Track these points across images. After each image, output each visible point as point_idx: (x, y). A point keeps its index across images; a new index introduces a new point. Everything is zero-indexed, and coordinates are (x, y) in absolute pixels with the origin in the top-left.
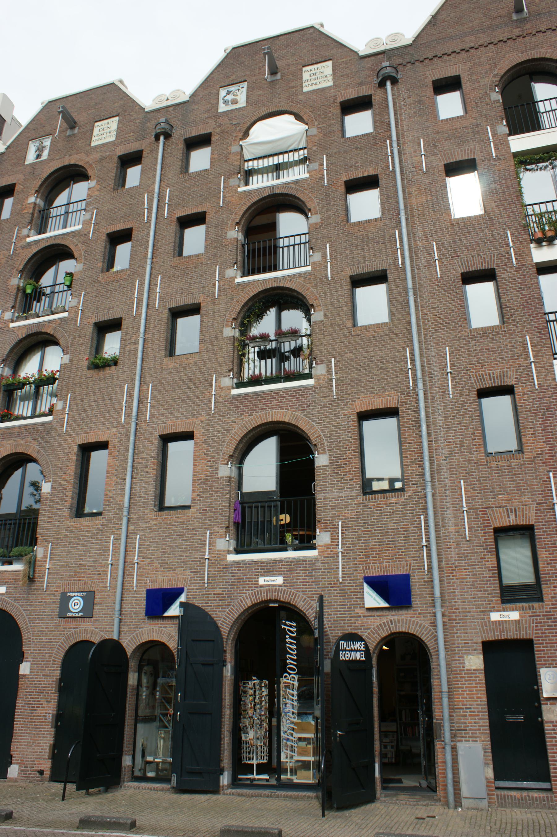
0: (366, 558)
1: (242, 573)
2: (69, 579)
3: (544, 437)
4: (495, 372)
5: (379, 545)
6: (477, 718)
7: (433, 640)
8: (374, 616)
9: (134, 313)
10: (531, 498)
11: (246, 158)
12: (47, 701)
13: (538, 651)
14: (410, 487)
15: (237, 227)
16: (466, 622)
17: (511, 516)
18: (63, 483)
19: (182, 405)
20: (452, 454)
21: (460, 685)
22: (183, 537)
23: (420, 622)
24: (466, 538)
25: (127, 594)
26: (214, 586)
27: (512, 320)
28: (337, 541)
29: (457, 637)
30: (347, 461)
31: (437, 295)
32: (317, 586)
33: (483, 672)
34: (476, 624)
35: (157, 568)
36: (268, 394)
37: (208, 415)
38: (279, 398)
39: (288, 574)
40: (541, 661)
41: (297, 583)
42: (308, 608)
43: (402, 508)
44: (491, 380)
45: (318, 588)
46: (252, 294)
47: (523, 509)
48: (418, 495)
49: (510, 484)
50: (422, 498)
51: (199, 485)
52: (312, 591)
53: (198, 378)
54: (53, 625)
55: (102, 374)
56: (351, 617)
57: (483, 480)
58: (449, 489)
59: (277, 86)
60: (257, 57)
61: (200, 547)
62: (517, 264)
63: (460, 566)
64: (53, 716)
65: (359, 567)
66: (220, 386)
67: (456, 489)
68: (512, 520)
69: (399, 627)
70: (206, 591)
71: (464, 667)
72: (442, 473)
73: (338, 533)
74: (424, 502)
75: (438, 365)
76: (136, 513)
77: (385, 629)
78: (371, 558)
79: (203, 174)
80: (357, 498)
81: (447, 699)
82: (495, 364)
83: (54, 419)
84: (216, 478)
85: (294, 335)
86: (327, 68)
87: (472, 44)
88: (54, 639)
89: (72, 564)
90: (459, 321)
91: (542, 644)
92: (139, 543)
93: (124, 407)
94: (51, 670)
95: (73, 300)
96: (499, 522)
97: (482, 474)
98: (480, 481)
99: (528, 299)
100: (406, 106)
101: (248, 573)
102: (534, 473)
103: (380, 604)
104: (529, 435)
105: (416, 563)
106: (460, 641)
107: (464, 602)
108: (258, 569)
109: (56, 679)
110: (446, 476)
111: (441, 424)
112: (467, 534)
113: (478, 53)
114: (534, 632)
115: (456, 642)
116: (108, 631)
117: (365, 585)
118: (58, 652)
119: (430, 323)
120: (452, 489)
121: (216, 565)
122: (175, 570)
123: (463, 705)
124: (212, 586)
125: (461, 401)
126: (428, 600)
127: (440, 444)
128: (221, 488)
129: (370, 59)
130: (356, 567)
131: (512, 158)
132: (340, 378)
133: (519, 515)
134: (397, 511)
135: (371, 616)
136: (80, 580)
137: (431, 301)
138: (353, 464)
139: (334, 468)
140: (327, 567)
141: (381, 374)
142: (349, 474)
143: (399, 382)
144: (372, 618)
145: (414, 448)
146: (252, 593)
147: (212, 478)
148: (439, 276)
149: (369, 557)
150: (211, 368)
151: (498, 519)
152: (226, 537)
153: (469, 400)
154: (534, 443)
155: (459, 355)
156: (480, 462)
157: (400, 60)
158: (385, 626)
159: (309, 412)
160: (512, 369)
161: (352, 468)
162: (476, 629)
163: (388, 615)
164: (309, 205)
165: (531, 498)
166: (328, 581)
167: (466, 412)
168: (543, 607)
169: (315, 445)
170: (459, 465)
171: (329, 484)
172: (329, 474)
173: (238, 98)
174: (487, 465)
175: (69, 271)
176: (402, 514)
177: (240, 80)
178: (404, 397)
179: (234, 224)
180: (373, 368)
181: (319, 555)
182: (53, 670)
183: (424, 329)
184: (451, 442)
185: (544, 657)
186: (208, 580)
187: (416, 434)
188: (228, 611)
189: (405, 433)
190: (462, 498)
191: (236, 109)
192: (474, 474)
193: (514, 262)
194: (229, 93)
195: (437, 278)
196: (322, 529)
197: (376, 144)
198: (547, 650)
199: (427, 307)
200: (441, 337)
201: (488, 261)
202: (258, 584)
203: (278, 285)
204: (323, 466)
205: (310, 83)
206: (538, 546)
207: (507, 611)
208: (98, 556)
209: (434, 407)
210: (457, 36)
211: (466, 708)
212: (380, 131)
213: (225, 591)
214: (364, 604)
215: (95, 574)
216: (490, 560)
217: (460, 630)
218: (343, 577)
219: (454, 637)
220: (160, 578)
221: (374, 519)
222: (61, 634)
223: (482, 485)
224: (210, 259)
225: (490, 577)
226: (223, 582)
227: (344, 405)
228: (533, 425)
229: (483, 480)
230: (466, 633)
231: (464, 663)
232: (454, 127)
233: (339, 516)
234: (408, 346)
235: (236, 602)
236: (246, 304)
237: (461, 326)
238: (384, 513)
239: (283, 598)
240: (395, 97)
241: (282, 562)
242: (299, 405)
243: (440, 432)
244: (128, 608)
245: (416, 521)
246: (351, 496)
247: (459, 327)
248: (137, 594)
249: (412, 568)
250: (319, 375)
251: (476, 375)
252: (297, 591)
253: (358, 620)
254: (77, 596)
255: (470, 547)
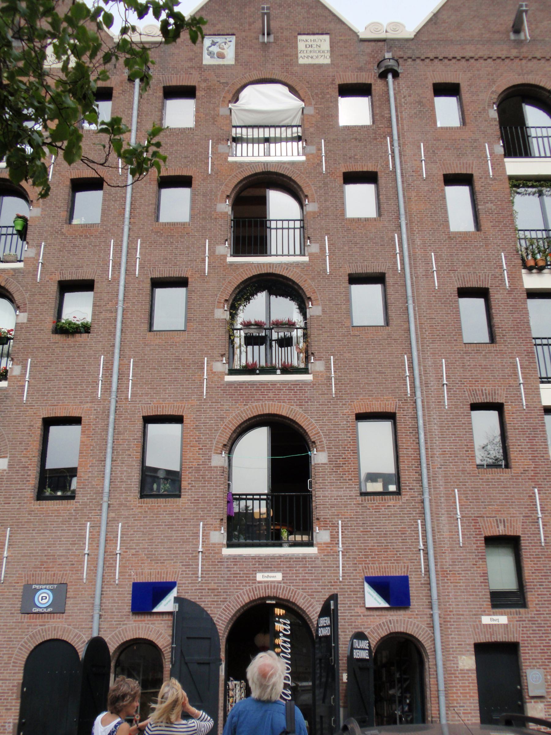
0: (365, 558)
1: (239, 568)
2: (33, 570)
3: (530, 455)
4: (487, 388)
5: (378, 546)
6: (469, 715)
7: (429, 641)
8: (374, 616)
9: (110, 277)
10: (518, 511)
11: (234, 124)
12: (6, 709)
13: (524, 653)
14: (408, 492)
15: (227, 201)
16: (460, 625)
17: (500, 527)
18: (23, 460)
19: (169, 386)
20: (446, 463)
21: (454, 685)
22: (173, 528)
23: (417, 623)
24: (459, 544)
25: (107, 588)
26: (208, 580)
27: (504, 341)
28: (337, 539)
29: (452, 638)
30: (346, 461)
31: (435, 306)
32: (317, 584)
33: (475, 672)
34: (469, 626)
35: (142, 560)
36: (264, 385)
37: (199, 400)
38: (275, 390)
39: (287, 570)
40: (526, 662)
41: (296, 580)
42: (308, 605)
43: (400, 511)
44: (483, 395)
45: (318, 586)
46: (246, 277)
47: (511, 520)
48: (415, 500)
49: (500, 496)
50: (419, 503)
51: (190, 473)
52: (312, 589)
53: (187, 359)
54: (13, 622)
55: (71, 340)
56: (351, 616)
57: (475, 491)
58: (443, 497)
59: (271, 50)
60: (247, 10)
61: (193, 539)
62: (509, 286)
63: (455, 571)
64: (14, 726)
65: (358, 567)
66: (212, 370)
67: (450, 497)
68: (501, 531)
69: (397, 627)
70: (199, 586)
71: (457, 667)
72: (437, 481)
73: (338, 532)
74: (420, 507)
75: (434, 375)
76: (117, 499)
77: (384, 628)
78: (370, 559)
79: (187, 132)
80: (356, 499)
81: (444, 698)
82: (487, 381)
83: (9, 386)
84: (208, 467)
85: (292, 326)
86: (324, 42)
87: (472, 54)
88: (14, 638)
89: (37, 553)
90: (455, 335)
91: (527, 647)
92: (121, 532)
93: (100, 381)
94: (10, 673)
95: (30, 249)
96: (490, 531)
97: (474, 485)
98: (472, 491)
99: (519, 323)
100: (406, 104)
101: (245, 568)
102: (521, 488)
103: (380, 604)
104: (516, 451)
105: (414, 565)
106: (454, 643)
107: (458, 605)
108: (256, 564)
109: (18, 683)
110: (441, 484)
111: (437, 433)
112: (461, 541)
113: (478, 64)
114: (521, 635)
115: (450, 643)
116: (83, 628)
117: (366, 585)
118: (21, 653)
119: (427, 333)
120: (447, 497)
121: (210, 559)
122: (164, 563)
123: (457, 703)
124: (205, 580)
125: (456, 413)
126: (424, 602)
127: (435, 452)
128: (214, 478)
129: (370, 43)
130: (356, 567)
131: (507, 181)
132: (339, 376)
133: (508, 526)
134: (395, 514)
135: (371, 616)
136: (48, 571)
137: (428, 311)
138: (352, 465)
139: (334, 467)
140: (327, 565)
141: (379, 378)
142: (348, 474)
143: (397, 388)
144: (371, 617)
145: (411, 454)
146: (249, 589)
147: (205, 467)
148: (437, 288)
149: (368, 558)
150: (202, 350)
151: (489, 528)
152: (221, 530)
153: (463, 413)
154: (521, 460)
155: (454, 368)
156: (473, 473)
157: (401, 53)
158: (384, 626)
159: (308, 408)
160: (503, 387)
161: (351, 469)
162: (469, 631)
163: (387, 615)
164: (306, 191)
165: (518, 511)
166: (328, 580)
167: (460, 424)
168: (528, 613)
169: (314, 442)
170: (453, 474)
171: (328, 483)
172: (328, 472)
173: (225, 52)
174: (478, 476)
175: (21, 214)
176: (400, 517)
177: (228, 32)
178: (402, 403)
179: (225, 196)
180: (371, 371)
181: (319, 552)
182: (14, 673)
183: (422, 339)
184: (445, 451)
185: (529, 659)
186: (202, 574)
187: (413, 441)
188: (223, 607)
189: (403, 438)
190: (456, 505)
191: (224, 65)
192: (467, 484)
193: (507, 285)
194: (214, 44)
195: (435, 289)
196: (322, 526)
197: (376, 139)
198: (532, 653)
199: (424, 316)
200: (437, 348)
201: (483, 280)
202: (256, 580)
203: (274, 272)
204: (322, 464)
205: (306, 55)
206: (524, 556)
207: (497, 615)
208: (71, 544)
209: (430, 416)
210: (457, 41)
211: (460, 706)
212: (380, 126)
213: (220, 586)
214: (364, 603)
215: (66, 564)
216: (481, 566)
217: (454, 631)
218: (343, 576)
219: (448, 638)
220: (146, 571)
221: (373, 520)
222: (24, 632)
223: (474, 495)
224: (198, 231)
225: (481, 582)
226: (218, 577)
227: (342, 405)
228: (520, 442)
229: (475, 491)
230: (460, 635)
231: (458, 664)
232: (453, 138)
233: (339, 515)
234: (406, 353)
235: (232, 597)
236: (238, 286)
237: (457, 340)
238: (383, 514)
239: (282, 594)
240: (396, 92)
241: (281, 559)
242: (297, 400)
243: (436, 440)
244: (109, 603)
245: (413, 525)
246: (350, 496)
247: (455, 340)
248: (119, 588)
249: (409, 570)
250: (318, 372)
251: (469, 389)
252: (297, 589)
253: (358, 619)
254: (46, 588)
255: (462, 553)
